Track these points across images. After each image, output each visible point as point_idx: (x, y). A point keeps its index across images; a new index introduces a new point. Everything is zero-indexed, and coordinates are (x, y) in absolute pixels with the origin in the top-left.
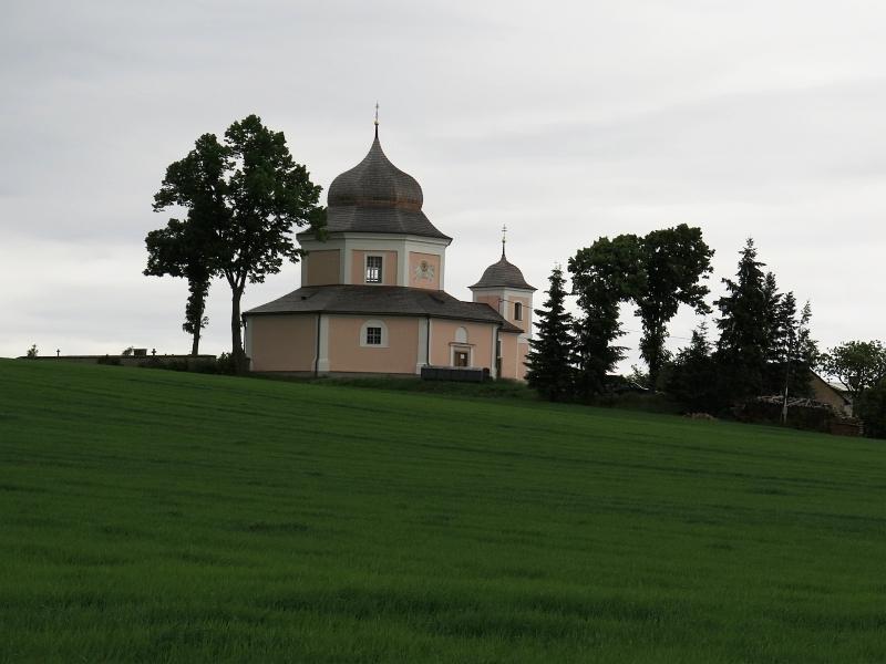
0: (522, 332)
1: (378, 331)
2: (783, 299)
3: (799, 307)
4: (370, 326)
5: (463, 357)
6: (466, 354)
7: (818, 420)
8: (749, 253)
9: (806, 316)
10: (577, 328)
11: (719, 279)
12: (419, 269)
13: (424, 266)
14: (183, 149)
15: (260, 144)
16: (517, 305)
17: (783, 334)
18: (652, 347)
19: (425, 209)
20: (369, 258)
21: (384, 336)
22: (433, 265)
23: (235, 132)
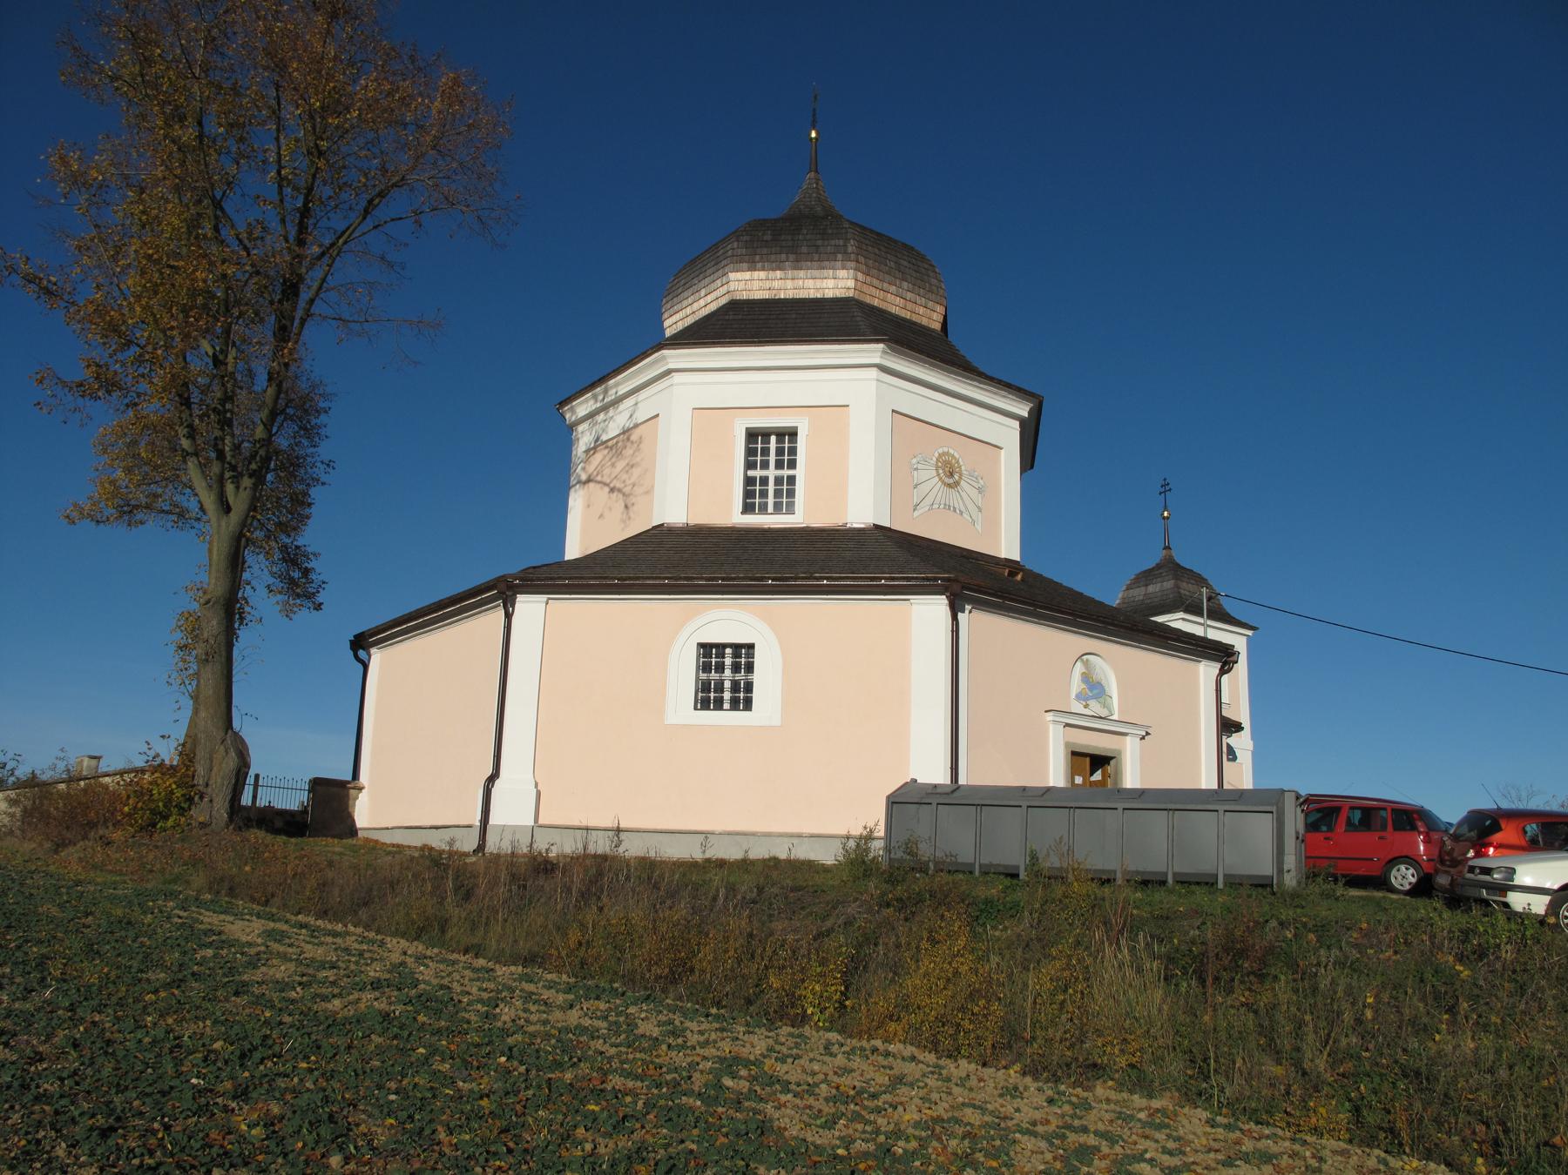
1: (744, 652)
20: (752, 435)
21: (766, 678)
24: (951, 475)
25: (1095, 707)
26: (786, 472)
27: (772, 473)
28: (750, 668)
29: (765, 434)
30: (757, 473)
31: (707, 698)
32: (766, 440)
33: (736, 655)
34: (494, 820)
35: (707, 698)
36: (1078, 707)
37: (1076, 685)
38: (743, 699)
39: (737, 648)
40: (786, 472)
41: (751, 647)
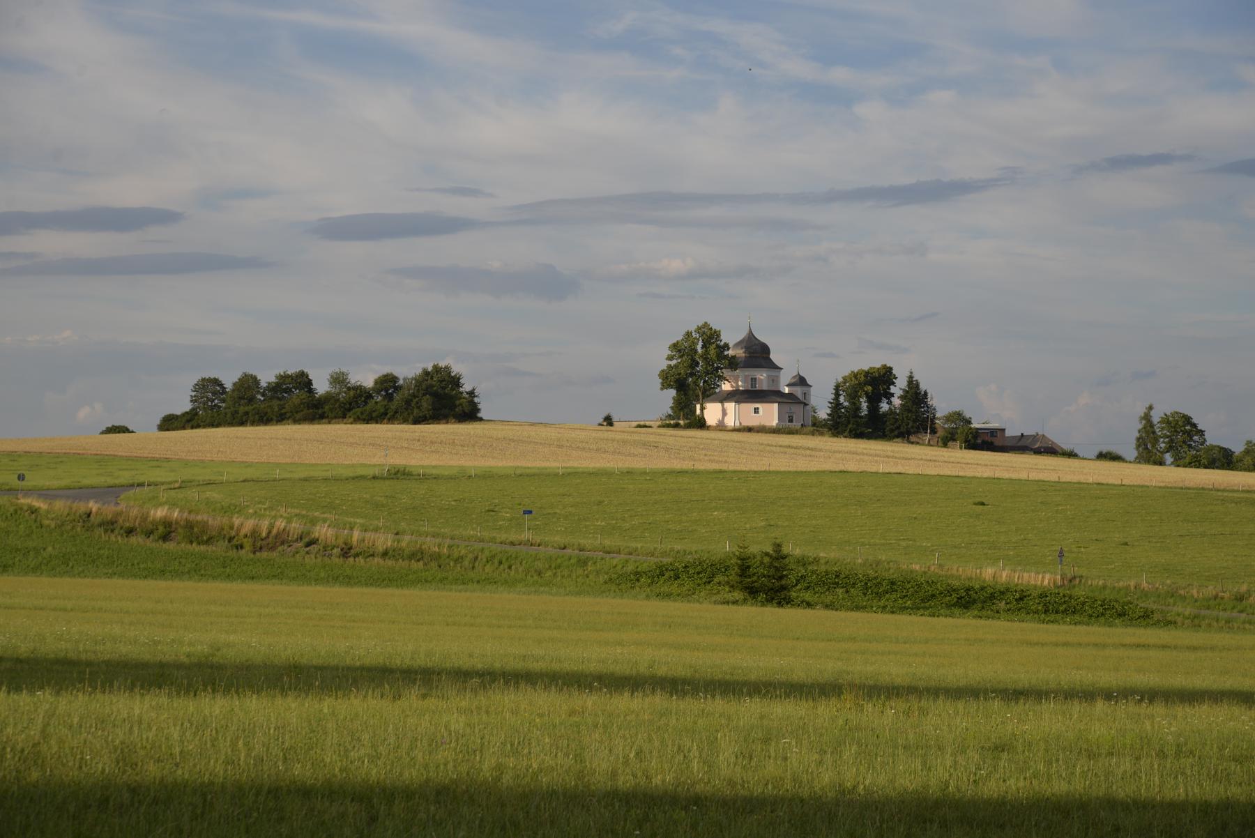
0: (807, 405)
1: (758, 408)
2: (923, 393)
3: (929, 396)
6: (792, 417)
7: (708, 428)
8: (911, 377)
9: (932, 398)
11: (898, 389)
13: (773, 380)
14: (675, 341)
15: (710, 336)
17: (923, 407)
19: (771, 356)
21: (761, 411)
22: (775, 380)
23: (699, 330)
31: (755, 413)
38: (758, 413)
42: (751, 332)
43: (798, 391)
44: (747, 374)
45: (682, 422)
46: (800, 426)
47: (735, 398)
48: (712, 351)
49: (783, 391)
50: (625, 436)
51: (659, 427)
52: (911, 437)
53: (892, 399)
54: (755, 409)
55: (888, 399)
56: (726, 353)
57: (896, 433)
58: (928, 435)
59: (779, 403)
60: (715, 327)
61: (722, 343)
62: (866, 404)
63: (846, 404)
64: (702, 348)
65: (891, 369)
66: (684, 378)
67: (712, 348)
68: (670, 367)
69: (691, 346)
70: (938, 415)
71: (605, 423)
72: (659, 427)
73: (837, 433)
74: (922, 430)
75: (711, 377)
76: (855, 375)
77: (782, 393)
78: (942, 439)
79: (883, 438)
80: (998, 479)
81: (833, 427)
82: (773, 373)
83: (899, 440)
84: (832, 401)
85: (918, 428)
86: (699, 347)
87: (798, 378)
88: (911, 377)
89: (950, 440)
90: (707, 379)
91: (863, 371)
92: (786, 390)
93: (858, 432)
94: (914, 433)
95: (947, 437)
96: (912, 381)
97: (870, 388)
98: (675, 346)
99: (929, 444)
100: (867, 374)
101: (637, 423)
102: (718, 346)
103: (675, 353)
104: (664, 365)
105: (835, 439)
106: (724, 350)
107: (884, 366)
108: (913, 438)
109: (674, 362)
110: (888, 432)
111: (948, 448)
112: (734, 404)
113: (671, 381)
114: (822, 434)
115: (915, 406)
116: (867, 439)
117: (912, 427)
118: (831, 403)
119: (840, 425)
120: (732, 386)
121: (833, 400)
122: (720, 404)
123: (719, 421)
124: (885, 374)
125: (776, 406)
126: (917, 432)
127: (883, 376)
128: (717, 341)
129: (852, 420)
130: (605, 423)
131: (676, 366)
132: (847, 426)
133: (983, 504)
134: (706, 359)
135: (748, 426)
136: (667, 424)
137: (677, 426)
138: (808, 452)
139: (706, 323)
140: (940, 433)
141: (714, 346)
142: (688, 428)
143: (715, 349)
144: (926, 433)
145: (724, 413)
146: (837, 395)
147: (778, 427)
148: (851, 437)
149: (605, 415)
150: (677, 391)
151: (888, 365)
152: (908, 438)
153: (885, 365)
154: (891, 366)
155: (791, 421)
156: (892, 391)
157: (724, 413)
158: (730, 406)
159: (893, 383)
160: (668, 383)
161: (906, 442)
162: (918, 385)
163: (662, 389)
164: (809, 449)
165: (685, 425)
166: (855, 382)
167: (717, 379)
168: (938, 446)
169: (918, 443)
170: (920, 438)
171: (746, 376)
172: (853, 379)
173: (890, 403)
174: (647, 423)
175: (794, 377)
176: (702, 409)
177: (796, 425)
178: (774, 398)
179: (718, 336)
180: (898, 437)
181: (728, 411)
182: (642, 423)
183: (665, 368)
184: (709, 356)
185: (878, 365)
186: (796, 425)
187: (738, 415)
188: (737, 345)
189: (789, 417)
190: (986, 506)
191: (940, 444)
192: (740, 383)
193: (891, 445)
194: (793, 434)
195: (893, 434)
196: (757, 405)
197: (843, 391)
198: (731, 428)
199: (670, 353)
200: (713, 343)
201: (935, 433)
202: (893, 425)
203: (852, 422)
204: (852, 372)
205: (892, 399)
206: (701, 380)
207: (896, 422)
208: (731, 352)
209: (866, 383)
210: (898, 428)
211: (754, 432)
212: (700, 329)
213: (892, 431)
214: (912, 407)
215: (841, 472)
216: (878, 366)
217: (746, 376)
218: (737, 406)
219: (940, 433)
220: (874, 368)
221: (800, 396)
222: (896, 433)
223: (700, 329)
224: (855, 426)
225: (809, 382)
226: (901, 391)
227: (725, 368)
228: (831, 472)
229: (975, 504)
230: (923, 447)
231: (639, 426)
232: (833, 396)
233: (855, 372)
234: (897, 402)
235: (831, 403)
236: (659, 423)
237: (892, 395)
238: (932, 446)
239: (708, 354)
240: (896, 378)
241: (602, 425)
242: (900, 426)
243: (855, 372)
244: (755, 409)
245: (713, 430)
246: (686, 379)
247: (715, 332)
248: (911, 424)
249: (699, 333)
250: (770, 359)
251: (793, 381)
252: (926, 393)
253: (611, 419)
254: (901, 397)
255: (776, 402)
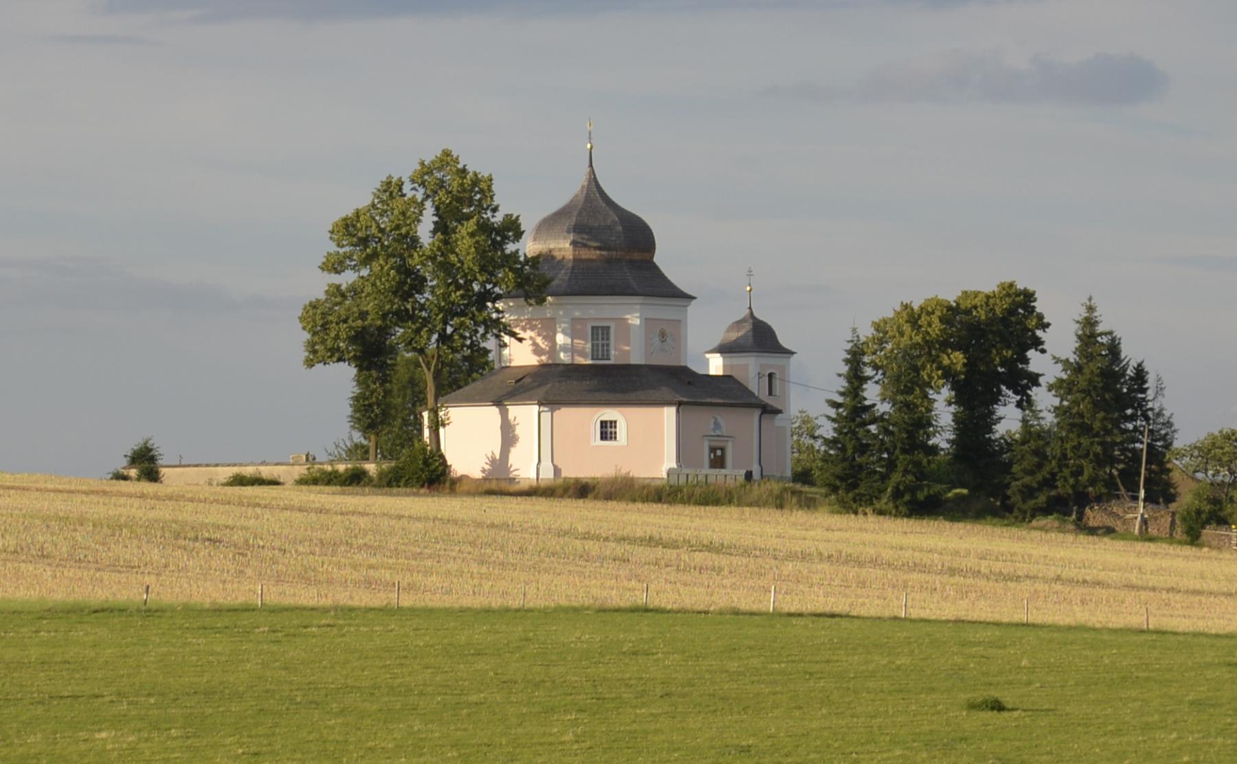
0: (778, 412)
1: (613, 424)
2: (1130, 372)
3: (1151, 383)
4: (605, 418)
5: (719, 453)
6: (723, 449)
8: (1089, 323)
10: (469, 185)
12: (657, 340)
13: (663, 335)
14: (349, 212)
16: (771, 376)
17: (1132, 418)
18: (877, 374)
19: (658, 259)
20: (593, 328)
21: (621, 430)
22: (667, 334)
23: (424, 175)
24: (663, 337)
25: (718, 433)
26: (605, 342)
27: (600, 342)
28: (615, 427)
29: (597, 327)
30: (604, 430)
31: (604, 437)
32: (603, 355)
33: (598, 355)
34: (541, 477)
35: (604, 437)
36: (713, 434)
37: (712, 426)
38: (613, 437)
39: (611, 422)
40: (605, 342)
41: (615, 422)
42: (593, 180)
43: (751, 369)
44: (577, 314)
45: (371, 468)
46: (741, 479)
47: (541, 392)
48: (465, 239)
49: (701, 371)
50: (188, 513)
51: (302, 482)
52: (1087, 510)
53: (1034, 392)
54: (604, 424)
55: (1022, 391)
56: (510, 248)
57: (1042, 499)
58: (1141, 504)
59: (679, 404)
60: (475, 164)
61: (498, 218)
62: (953, 408)
63: (884, 408)
64: (434, 232)
65: (1029, 296)
66: (380, 329)
67: (464, 233)
68: (337, 292)
69: (398, 227)
70: (1177, 444)
71: (133, 472)
72: (302, 482)
73: (855, 501)
74: (1123, 491)
75: (462, 324)
76: (913, 318)
77: (693, 374)
78: (1184, 519)
79: (1003, 517)
80: (1160, 632)
81: (842, 479)
82: (663, 310)
83: (1050, 520)
84: (840, 400)
85: (1110, 484)
86: (425, 231)
87: (748, 327)
88: (1089, 323)
89: (1208, 522)
90: (449, 330)
91: (939, 303)
92: (716, 365)
93: (921, 496)
94: (1099, 499)
95: (1199, 512)
96: (1093, 336)
97: (957, 359)
98: (348, 228)
99: (1145, 537)
100: (952, 313)
101: (227, 472)
102: (485, 228)
103: (347, 249)
104: (317, 285)
105: (849, 521)
106: (505, 238)
107: (1009, 289)
108: (1094, 516)
109: (347, 278)
110: (1019, 497)
111: (1201, 546)
112: (536, 408)
113: (337, 337)
114: (808, 504)
115: (1101, 415)
116: (946, 519)
117: (1093, 481)
118: (836, 405)
119: (863, 475)
120: (537, 351)
121: (842, 394)
122: (493, 412)
123: (493, 461)
124: (1011, 312)
125: (669, 413)
126: (1109, 493)
127: (1004, 320)
128: (481, 208)
129: (902, 459)
130: (133, 472)
131: (355, 291)
132: (884, 478)
133: (998, 706)
134: (446, 268)
135: (577, 480)
136: (324, 472)
137: (356, 479)
138: (699, 557)
139: (447, 153)
140: (1186, 499)
141: (471, 225)
142: (389, 485)
143: (472, 235)
144: (1135, 498)
145: (509, 436)
146: (856, 379)
147: (674, 481)
148: (898, 514)
149: (132, 444)
150: (360, 368)
151: (1020, 286)
152: (1080, 516)
153: (1011, 285)
154: (1031, 288)
155: (718, 462)
156: (1033, 367)
157: (509, 436)
158: (525, 415)
159: (1037, 343)
160: (329, 343)
161: (1072, 527)
162: (1114, 349)
163: (310, 363)
164: (710, 548)
165: (381, 475)
166: (911, 337)
167: (481, 330)
168: (1171, 540)
169: (1109, 531)
170: (1112, 514)
171: (574, 321)
172: (907, 328)
173: (1025, 403)
174: (266, 472)
175: (739, 323)
176: (436, 425)
177: (731, 475)
178: (665, 392)
179: (487, 193)
180: (1046, 511)
181: (519, 431)
182: (249, 471)
183: (323, 297)
184: (453, 258)
185: (987, 283)
186: (731, 475)
187: (550, 443)
188: (549, 224)
189: (713, 450)
190: (1005, 714)
191: (1179, 533)
192: (561, 339)
193: (1020, 539)
194: (717, 502)
195: (1031, 503)
196: (609, 414)
197: (876, 367)
198: (524, 486)
199: (333, 248)
200: (468, 217)
201: (1170, 499)
202: (1031, 473)
203: (900, 468)
204: (906, 307)
205: (1034, 392)
206: (431, 332)
207: (1040, 466)
208: (528, 247)
209: (945, 345)
210: (1049, 483)
211: (596, 498)
212: (430, 173)
213: (1029, 493)
214: (1093, 416)
215: (634, 610)
216: (989, 286)
217: (574, 321)
218: (546, 416)
219: (1186, 499)
220: (976, 294)
221: (756, 387)
222: (1042, 499)
223: (430, 173)
224: (910, 477)
225: (784, 340)
226: (1060, 366)
227: (508, 295)
228: (602, 610)
229: (973, 706)
230: (1120, 544)
231: (239, 481)
232: (842, 384)
233: (916, 307)
234: (1045, 400)
235: (836, 405)
236: (300, 471)
237: (1034, 379)
238: (1151, 539)
239: (453, 252)
240: (1045, 326)
241: (125, 478)
242: (1053, 475)
243: (916, 307)
244: (604, 424)
245: (469, 494)
246: (384, 331)
247: (476, 181)
248: (1088, 472)
249: (423, 184)
250: (654, 264)
251: (734, 336)
252: (1140, 375)
253: (152, 459)
254: (1059, 387)
255: (669, 404)
